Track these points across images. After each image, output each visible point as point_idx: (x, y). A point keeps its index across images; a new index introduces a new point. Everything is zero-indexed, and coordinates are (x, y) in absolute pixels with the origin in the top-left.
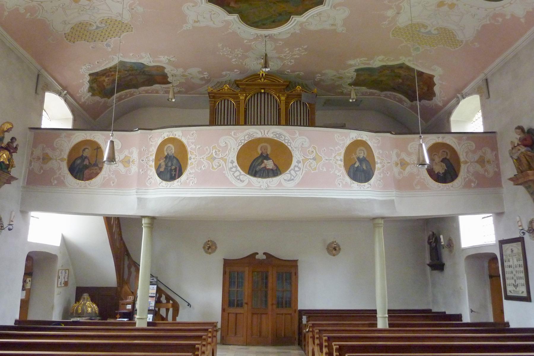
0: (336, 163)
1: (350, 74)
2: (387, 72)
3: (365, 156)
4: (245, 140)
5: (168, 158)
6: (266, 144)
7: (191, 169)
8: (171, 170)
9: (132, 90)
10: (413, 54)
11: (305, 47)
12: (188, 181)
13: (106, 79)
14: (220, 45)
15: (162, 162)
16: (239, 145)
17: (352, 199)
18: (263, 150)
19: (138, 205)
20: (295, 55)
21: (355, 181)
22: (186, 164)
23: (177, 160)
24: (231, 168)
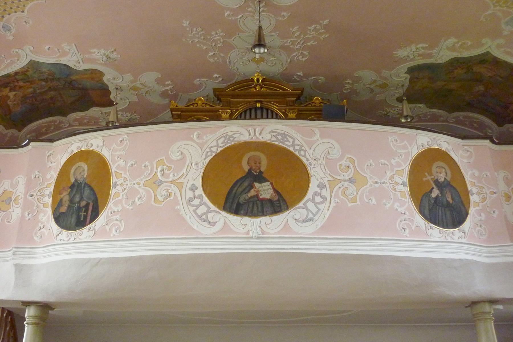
0: (394, 189)
1: (400, 76)
2: (460, 72)
3: (449, 178)
4: (218, 146)
5: (76, 187)
6: (257, 153)
7: (115, 204)
8: (79, 209)
9: (57, 119)
10: (505, 33)
11: (326, 22)
12: (108, 228)
13: (11, 94)
14: (186, 23)
15: (65, 196)
16: (207, 156)
17: (432, 259)
18: (253, 164)
19: (16, 279)
20: (309, 40)
21: (435, 224)
22: (107, 195)
23: (92, 189)
24: (191, 200)
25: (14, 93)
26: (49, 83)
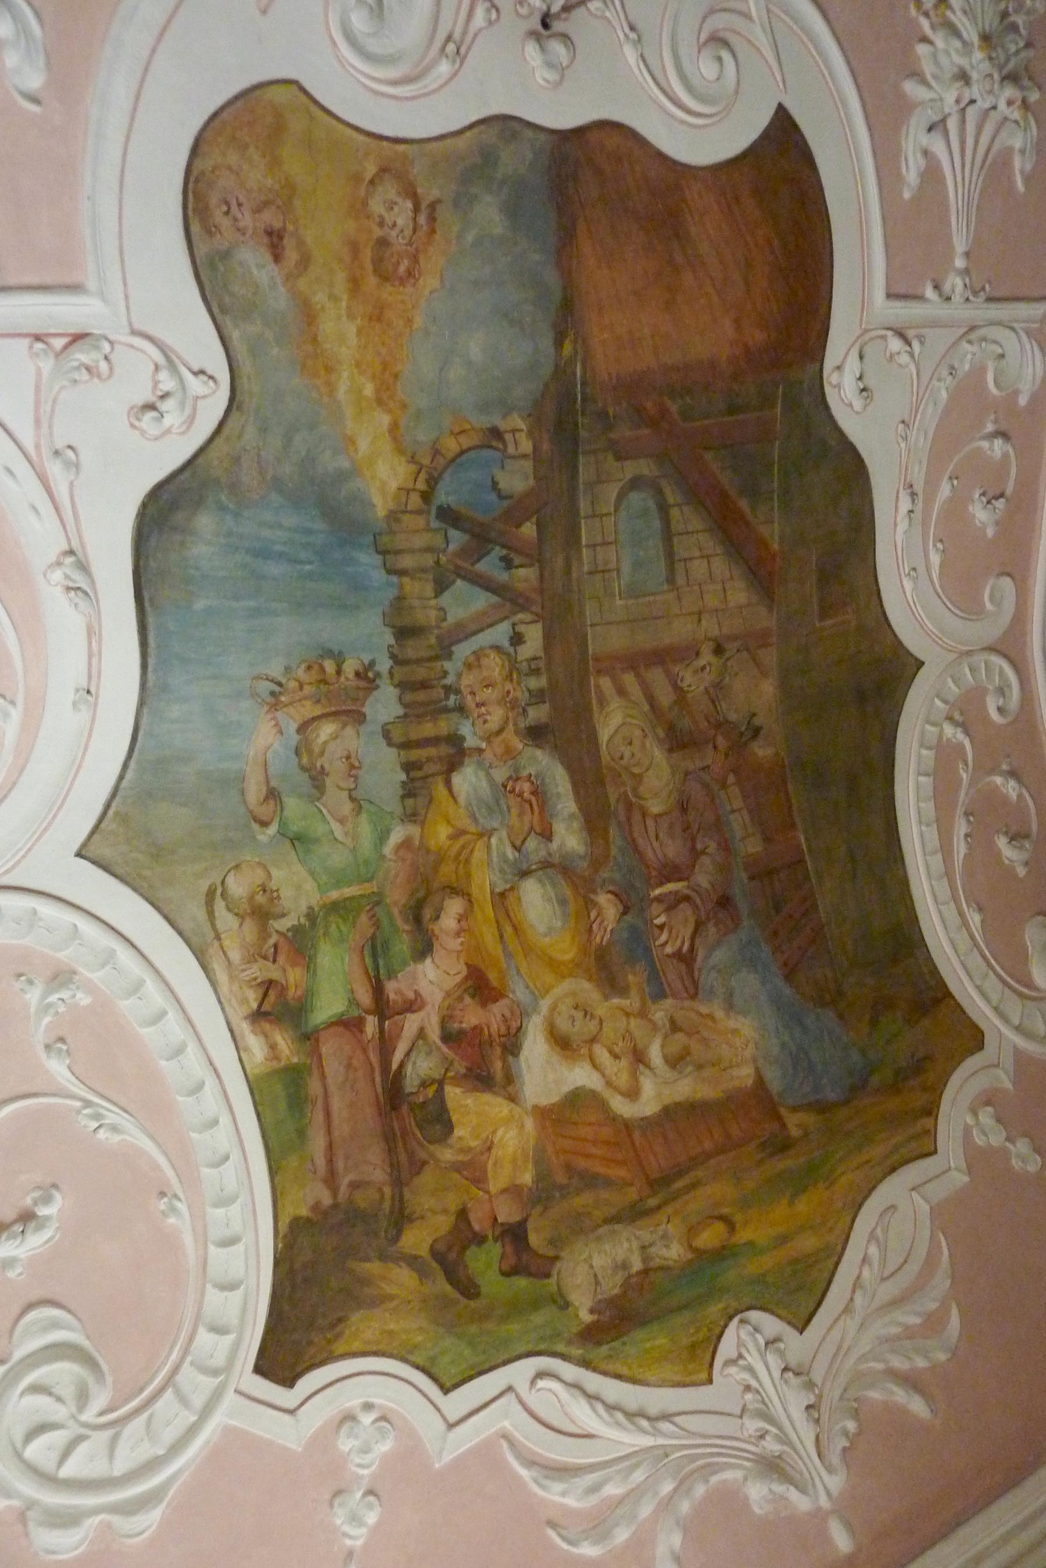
13: (543, 1073)
25: (535, 1048)
26: (469, 734)
